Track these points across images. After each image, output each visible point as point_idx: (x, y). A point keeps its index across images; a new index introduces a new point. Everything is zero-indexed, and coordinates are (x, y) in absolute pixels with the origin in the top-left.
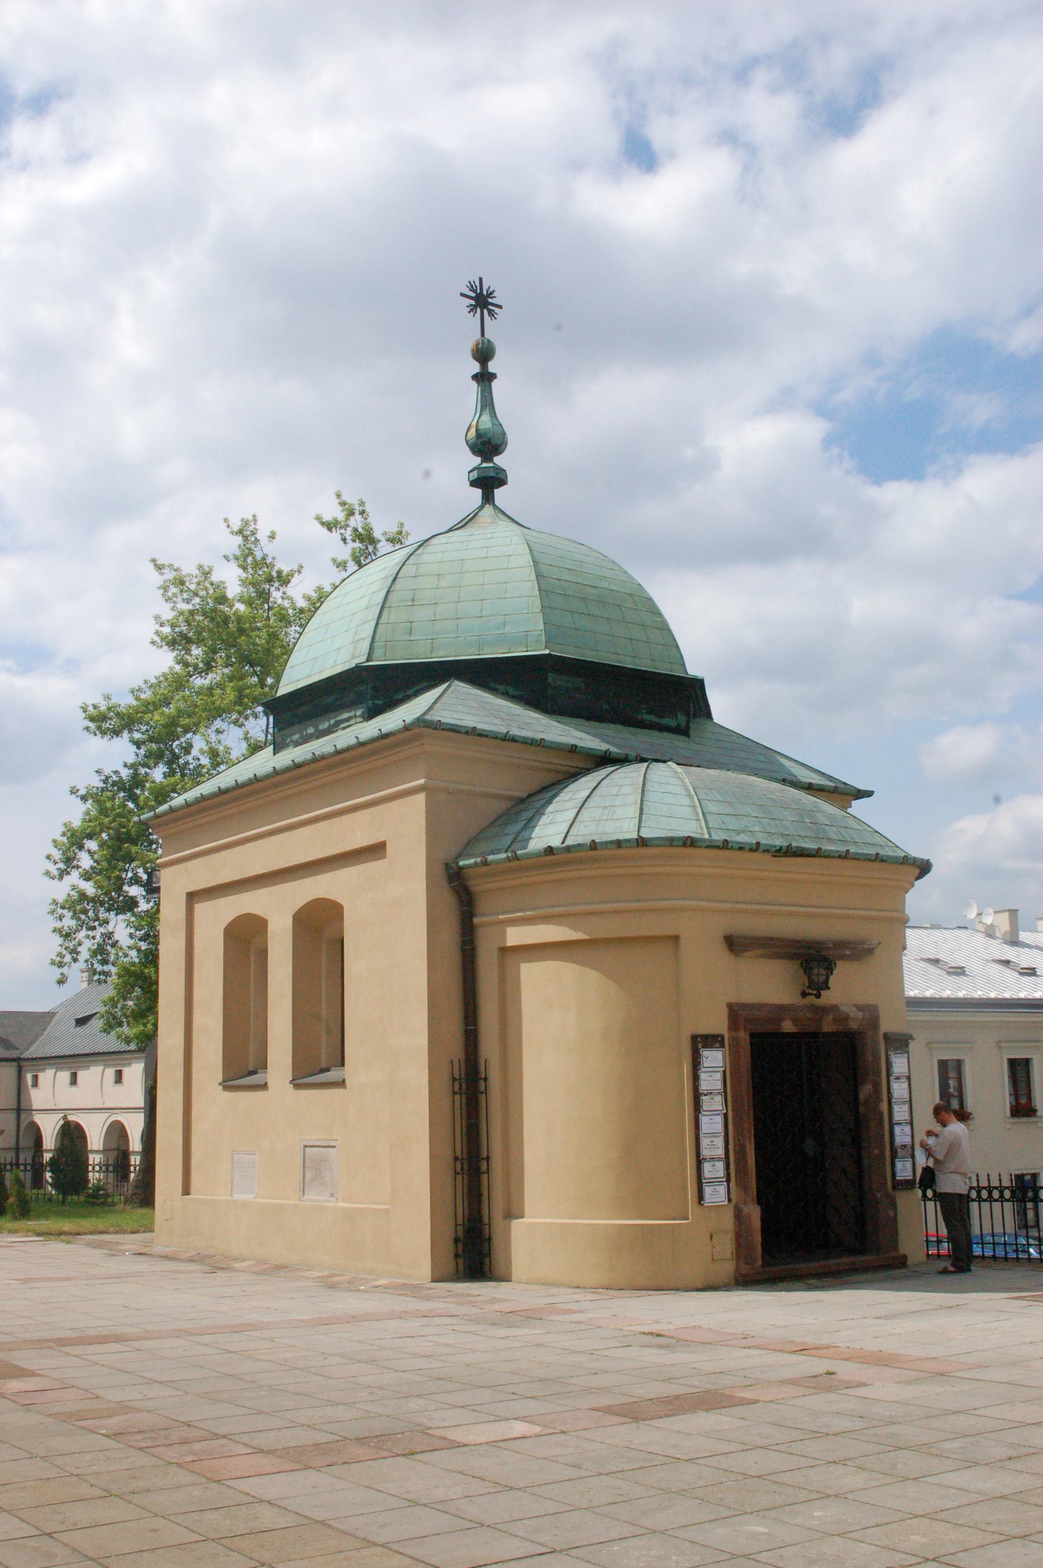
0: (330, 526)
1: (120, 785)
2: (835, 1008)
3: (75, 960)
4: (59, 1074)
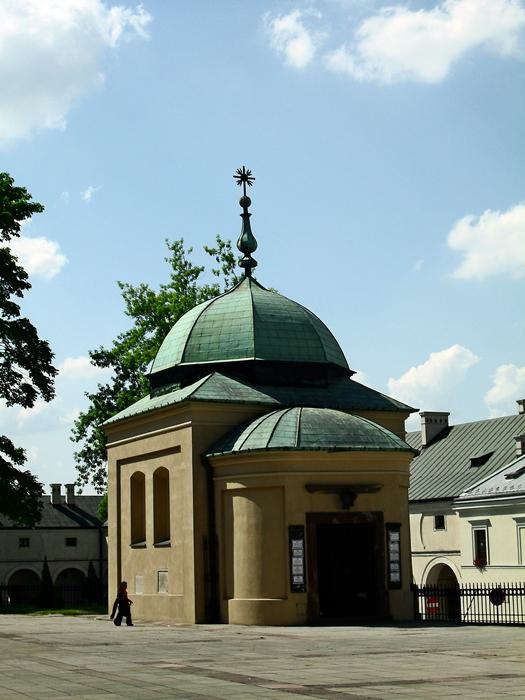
0: (211, 252)
1: (108, 391)
2: (360, 513)
3: (87, 483)
4: (425, 518)
